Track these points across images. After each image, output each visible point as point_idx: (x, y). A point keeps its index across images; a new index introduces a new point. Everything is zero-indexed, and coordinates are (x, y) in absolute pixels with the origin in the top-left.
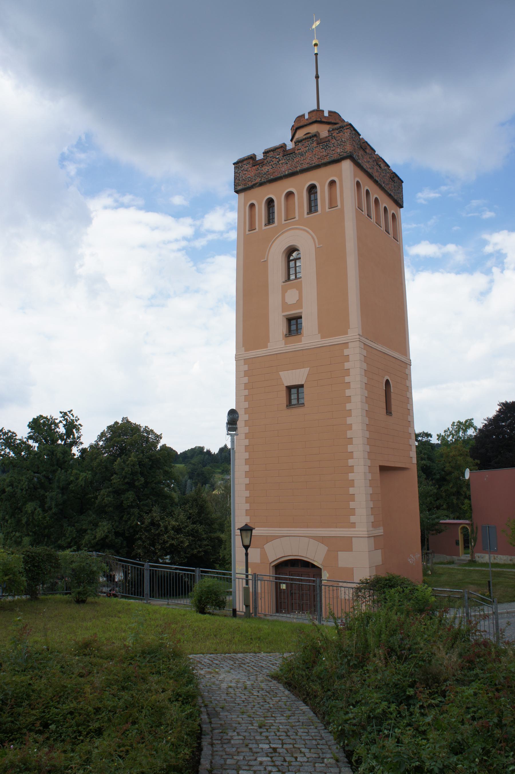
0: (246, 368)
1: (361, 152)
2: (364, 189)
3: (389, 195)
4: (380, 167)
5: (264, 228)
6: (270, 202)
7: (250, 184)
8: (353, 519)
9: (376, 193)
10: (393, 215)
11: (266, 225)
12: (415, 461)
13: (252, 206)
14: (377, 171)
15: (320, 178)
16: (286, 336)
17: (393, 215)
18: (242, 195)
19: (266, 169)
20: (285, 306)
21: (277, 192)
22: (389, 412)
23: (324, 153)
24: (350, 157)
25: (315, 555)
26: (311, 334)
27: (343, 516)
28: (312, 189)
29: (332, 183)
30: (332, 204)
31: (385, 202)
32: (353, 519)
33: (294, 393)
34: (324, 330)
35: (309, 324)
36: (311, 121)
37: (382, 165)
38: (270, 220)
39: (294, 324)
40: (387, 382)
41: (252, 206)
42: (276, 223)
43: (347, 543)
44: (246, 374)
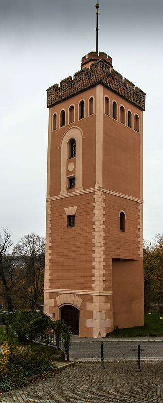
0: (50, 206)
1: (109, 79)
2: (111, 101)
3: (134, 104)
4: (126, 87)
5: (60, 128)
6: (63, 112)
7: (54, 102)
8: (93, 286)
9: (121, 103)
10: (136, 117)
11: (61, 127)
12: (142, 256)
13: (55, 115)
14: (123, 89)
15: (85, 97)
16: (68, 189)
17: (136, 117)
18: (51, 109)
19: (61, 92)
20: (68, 172)
21: (65, 107)
22: (122, 228)
23: (88, 81)
24: (101, 82)
25: (77, 303)
26: (79, 189)
27: (89, 285)
28: (82, 104)
29: (92, 100)
30: (91, 113)
31: (129, 108)
32: (93, 286)
33: (71, 219)
34: (85, 186)
35: (79, 182)
36: (89, 60)
37: (128, 85)
38: (63, 124)
39: (72, 181)
40: (122, 214)
41: (55, 115)
42: (65, 126)
43: (89, 298)
44: (51, 209)
